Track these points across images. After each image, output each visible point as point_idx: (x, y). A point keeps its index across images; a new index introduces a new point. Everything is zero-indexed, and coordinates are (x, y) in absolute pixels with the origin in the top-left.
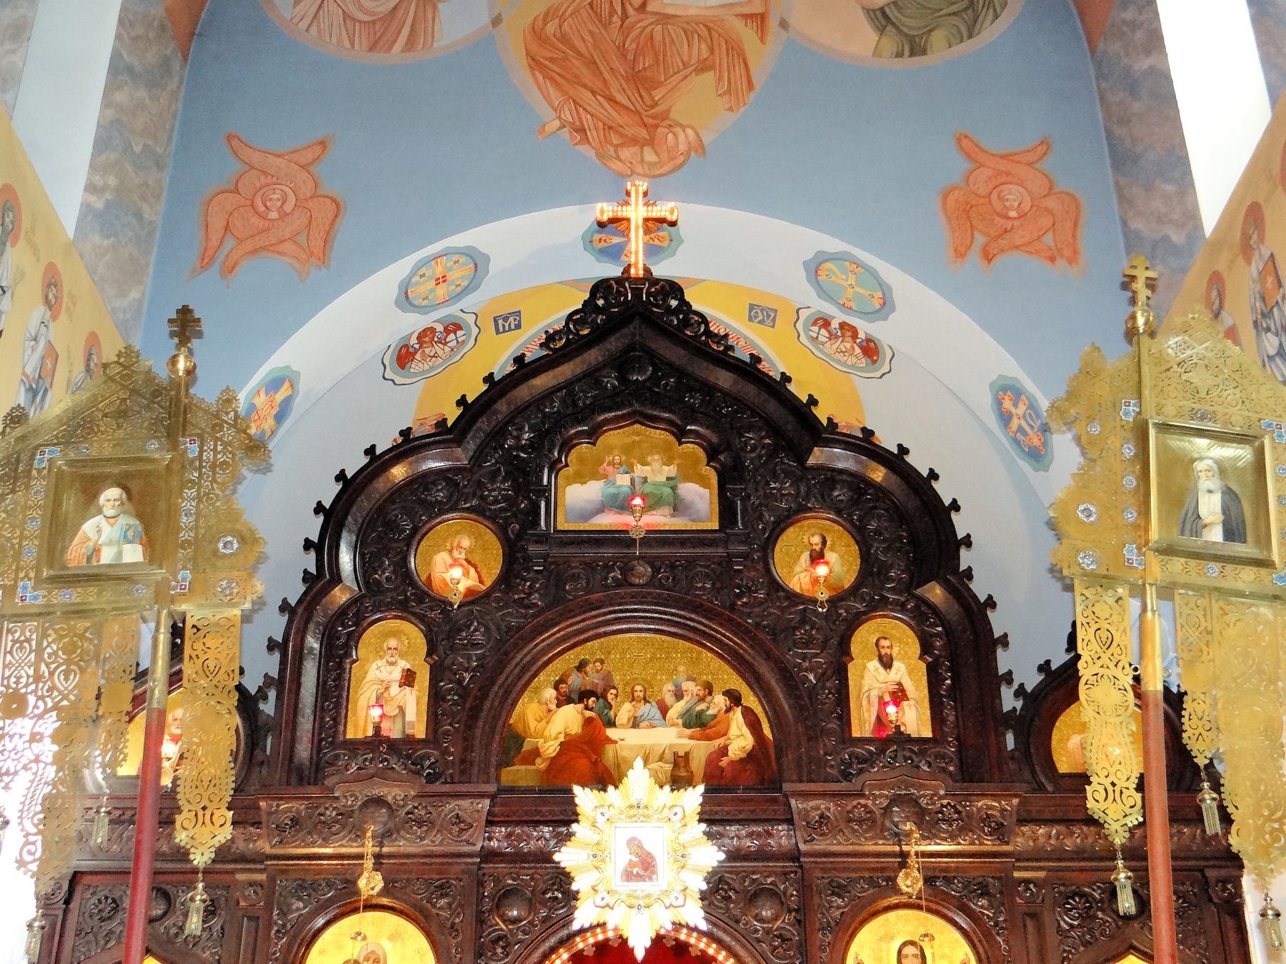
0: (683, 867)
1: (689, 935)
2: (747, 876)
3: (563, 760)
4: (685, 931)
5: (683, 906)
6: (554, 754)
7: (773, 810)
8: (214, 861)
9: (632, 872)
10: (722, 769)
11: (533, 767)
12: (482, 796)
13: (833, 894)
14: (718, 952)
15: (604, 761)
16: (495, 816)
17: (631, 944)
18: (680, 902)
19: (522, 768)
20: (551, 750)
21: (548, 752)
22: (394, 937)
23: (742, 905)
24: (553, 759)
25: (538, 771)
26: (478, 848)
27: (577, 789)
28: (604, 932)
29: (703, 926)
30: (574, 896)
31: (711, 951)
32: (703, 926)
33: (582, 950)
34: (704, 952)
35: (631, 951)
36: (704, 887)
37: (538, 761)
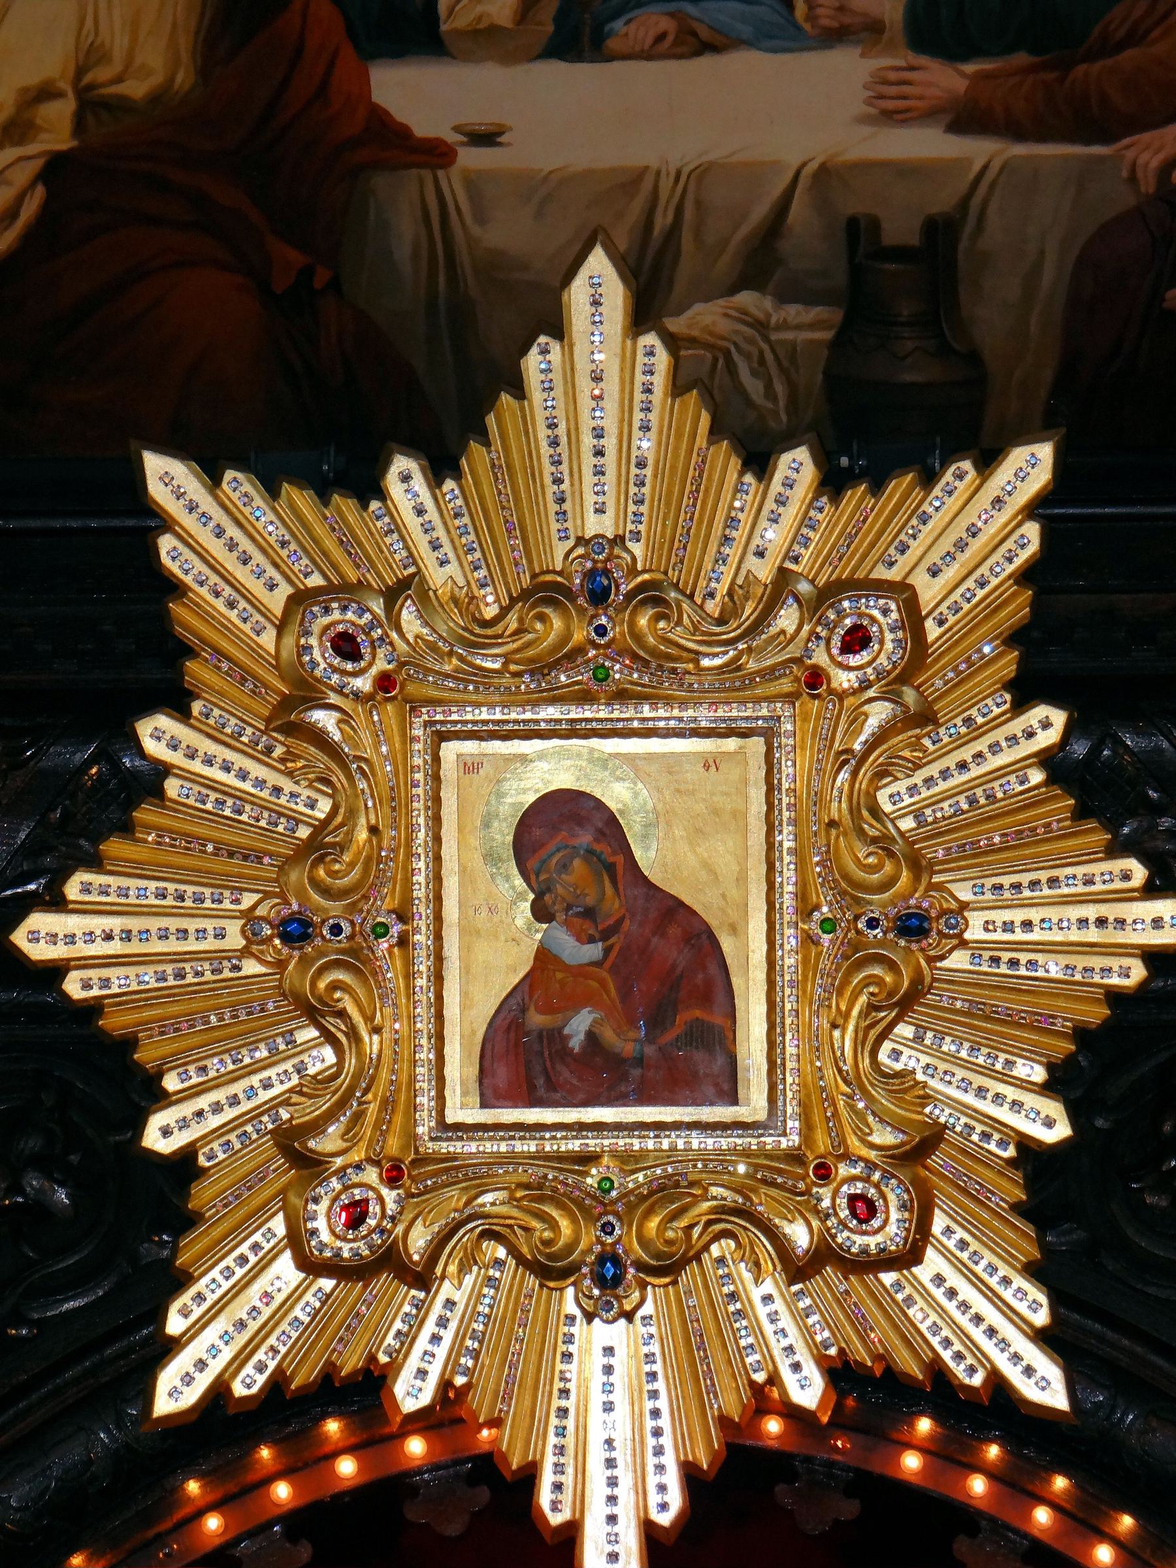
9: (555, 1038)
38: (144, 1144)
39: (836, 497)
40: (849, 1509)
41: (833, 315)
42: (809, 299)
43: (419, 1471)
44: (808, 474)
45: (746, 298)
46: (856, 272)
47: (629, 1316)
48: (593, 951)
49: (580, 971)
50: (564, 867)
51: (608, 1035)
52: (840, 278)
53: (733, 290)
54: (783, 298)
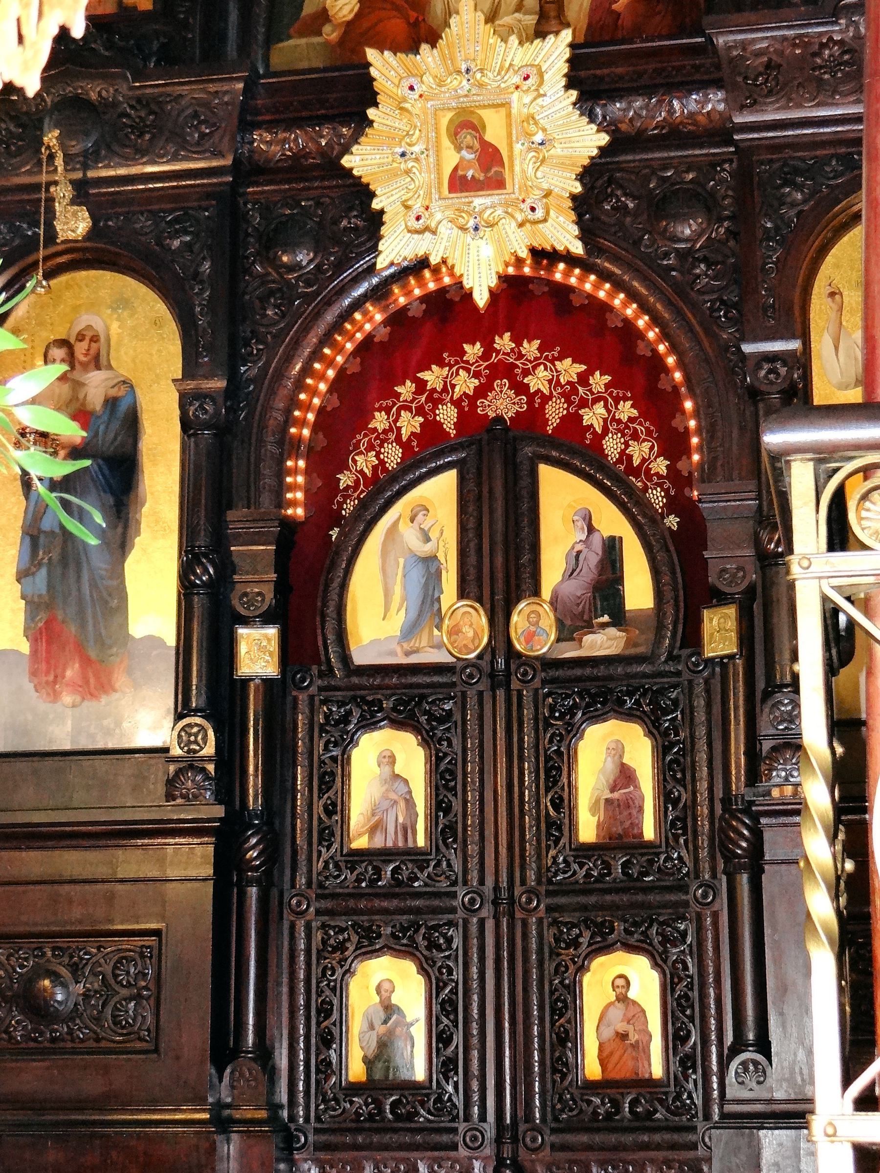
0: (543, 161)
1: (567, 274)
2: (654, 172)
3: (366, 25)
4: (561, 266)
5: (545, 220)
6: (350, 17)
7: (694, 66)
8: (480, 600)
9: (464, 177)
10: (618, 15)
11: (316, 40)
12: (238, 79)
13: (786, 183)
14: (649, 327)
15: (430, 21)
16: (258, 112)
17: (467, 284)
18: (539, 214)
19: (303, 41)
20: (345, 11)
21: (341, 14)
22: (122, 303)
23: (645, 217)
24: (349, 24)
25: (327, 43)
26: (228, 161)
27: (372, 54)
28: (437, 278)
29: (578, 248)
30: (376, 220)
31: (641, 323)
32: (578, 248)
33: (404, 309)
34: (591, 297)
35: (468, 296)
36: (577, 188)
37: (327, 29)
38: (706, 613)
39: (522, 46)
40: (546, 289)
41: (537, 17)
42: (530, 14)
43: (449, 286)
44: (517, 42)
45: (517, 15)
46: (541, 7)
47: (482, 238)
48: (473, 156)
49: (469, 161)
50: (465, 137)
51: (477, 175)
52: (538, 9)
53: (513, 13)
54: (525, 14)
